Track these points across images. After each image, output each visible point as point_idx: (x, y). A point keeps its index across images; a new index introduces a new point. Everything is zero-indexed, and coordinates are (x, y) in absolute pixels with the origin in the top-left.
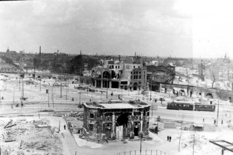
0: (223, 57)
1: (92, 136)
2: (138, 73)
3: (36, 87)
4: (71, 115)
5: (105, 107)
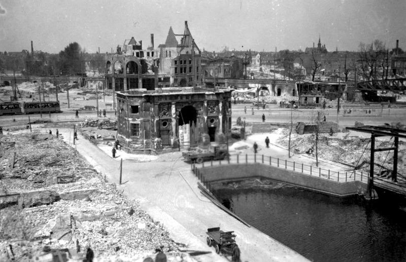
2: (187, 62)
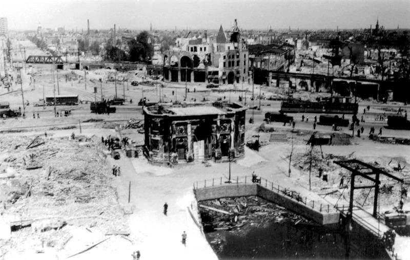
0: (374, 27)
2: (235, 57)
3: (80, 84)
4: (129, 126)
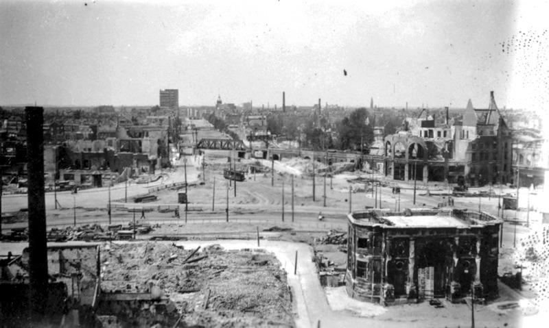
1: (364, 289)
5: (394, 225)
